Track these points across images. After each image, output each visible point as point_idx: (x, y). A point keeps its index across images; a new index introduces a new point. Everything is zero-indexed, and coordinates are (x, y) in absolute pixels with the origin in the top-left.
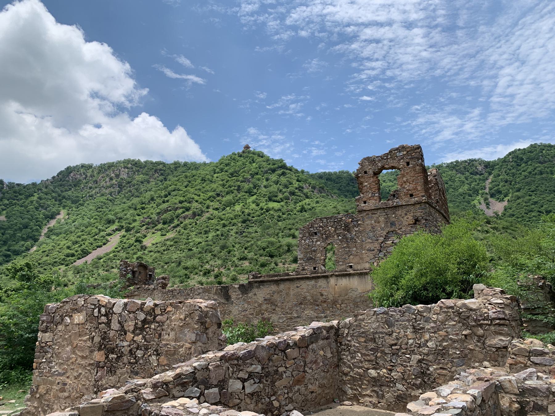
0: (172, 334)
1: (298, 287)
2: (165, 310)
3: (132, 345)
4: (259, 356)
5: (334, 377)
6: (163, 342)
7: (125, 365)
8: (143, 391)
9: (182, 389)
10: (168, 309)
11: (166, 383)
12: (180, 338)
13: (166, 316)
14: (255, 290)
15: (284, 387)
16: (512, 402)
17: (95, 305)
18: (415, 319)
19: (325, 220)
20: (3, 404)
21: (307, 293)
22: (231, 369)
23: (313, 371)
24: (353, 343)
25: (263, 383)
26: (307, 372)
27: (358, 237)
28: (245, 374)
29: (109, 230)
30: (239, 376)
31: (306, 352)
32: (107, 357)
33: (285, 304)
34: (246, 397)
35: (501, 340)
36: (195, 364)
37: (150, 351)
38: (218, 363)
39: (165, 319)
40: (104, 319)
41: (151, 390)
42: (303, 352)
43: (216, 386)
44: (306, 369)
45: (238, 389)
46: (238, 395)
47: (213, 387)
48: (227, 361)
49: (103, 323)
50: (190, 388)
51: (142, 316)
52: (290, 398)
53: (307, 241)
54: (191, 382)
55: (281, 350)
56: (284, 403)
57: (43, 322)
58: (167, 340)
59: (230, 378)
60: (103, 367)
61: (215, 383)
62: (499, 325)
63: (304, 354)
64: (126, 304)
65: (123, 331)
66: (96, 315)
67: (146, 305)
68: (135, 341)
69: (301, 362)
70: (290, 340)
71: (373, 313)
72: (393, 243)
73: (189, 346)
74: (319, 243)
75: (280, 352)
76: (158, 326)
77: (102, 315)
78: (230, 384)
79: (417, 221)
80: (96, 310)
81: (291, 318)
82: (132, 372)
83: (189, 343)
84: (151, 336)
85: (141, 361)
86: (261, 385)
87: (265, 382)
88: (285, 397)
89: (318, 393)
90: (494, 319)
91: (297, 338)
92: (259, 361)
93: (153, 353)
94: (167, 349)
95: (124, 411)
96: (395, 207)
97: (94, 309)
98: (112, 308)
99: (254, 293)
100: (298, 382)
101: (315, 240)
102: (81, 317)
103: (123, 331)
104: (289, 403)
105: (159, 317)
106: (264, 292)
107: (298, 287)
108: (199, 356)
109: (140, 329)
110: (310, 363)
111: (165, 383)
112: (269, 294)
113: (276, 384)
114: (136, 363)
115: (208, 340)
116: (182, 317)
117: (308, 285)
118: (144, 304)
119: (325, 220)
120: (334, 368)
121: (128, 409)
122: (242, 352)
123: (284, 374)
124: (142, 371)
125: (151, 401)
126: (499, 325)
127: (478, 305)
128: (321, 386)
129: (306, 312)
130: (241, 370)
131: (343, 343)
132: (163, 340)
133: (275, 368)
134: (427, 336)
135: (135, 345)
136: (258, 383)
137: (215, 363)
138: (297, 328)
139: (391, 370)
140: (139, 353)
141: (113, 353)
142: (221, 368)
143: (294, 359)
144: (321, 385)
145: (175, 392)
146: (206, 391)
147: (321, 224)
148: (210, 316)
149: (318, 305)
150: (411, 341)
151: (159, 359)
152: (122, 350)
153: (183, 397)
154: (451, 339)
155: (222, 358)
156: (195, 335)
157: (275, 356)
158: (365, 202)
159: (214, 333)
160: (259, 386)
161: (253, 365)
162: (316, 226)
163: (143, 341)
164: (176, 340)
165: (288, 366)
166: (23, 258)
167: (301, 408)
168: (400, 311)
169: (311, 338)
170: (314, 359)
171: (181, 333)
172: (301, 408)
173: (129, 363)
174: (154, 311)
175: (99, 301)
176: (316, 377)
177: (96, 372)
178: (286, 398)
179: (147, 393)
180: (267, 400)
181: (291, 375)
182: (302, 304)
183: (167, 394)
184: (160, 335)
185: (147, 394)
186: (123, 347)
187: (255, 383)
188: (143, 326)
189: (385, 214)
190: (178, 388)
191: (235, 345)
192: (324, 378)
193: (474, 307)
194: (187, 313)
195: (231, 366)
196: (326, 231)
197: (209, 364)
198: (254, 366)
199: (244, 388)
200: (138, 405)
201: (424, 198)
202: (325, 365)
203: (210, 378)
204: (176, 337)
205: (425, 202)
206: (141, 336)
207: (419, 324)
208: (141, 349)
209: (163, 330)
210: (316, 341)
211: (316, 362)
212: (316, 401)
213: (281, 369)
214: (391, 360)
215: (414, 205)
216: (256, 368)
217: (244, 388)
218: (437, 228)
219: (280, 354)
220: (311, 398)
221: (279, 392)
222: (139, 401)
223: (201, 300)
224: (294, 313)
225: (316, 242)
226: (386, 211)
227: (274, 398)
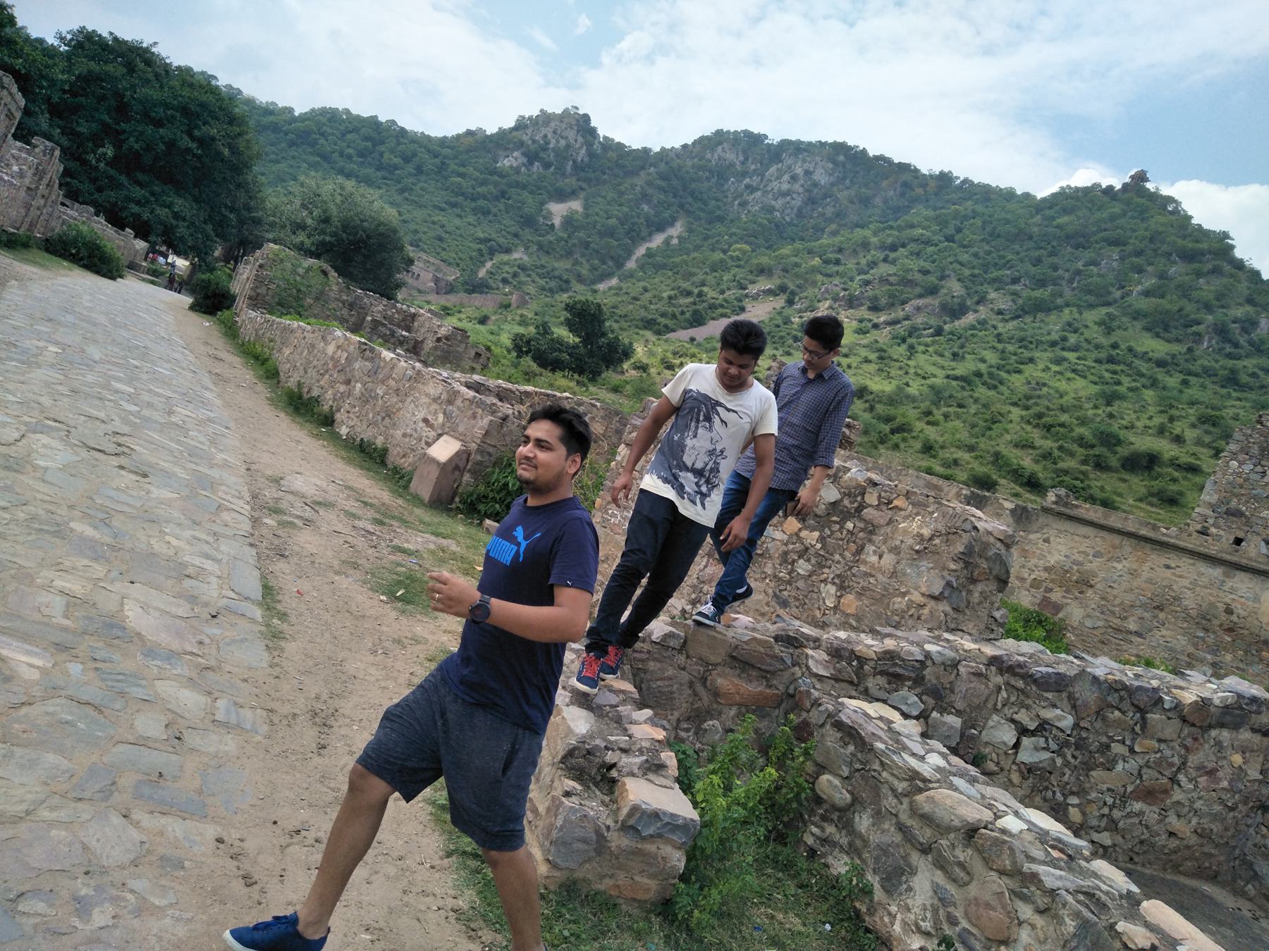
0: (888, 560)
1: (1168, 567)
2: (890, 502)
3: (793, 543)
4: (1077, 695)
5: (1243, 827)
6: (863, 568)
7: (765, 578)
8: (810, 652)
9: (887, 686)
10: (896, 503)
12: (905, 574)
15: (1109, 790)
20: (365, 503)
21: (1189, 592)
22: (1004, 694)
23: (1195, 790)
25: (1064, 756)
26: (1180, 786)
28: (1031, 719)
29: (753, 289)
30: (1016, 717)
31: (1195, 739)
33: (1115, 592)
34: (1014, 767)
37: (828, 573)
38: (983, 668)
39: (882, 522)
41: (826, 658)
42: (1189, 735)
43: (959, 713)
45: (1005, 744)
46: (998, 755)
47: (952, 713)
48: (1001, 671)
50: (904, 692)
52: (1113, 821)
54: (909, 679)
55: (1136, 707)
56: (1094, 822)
58: (873, 567)
59: (996, 710)
63: (1189, 742)
67: (849, 475)
69: (1173, 756)
70: (1167, 694)
73: (921, 600)
75: (1132, 708)
76: (862, 530)
78: (991, 723)
81: (1118, 630)
82: (775, 595)
83: (923, 595)
84: (841, 543)
85: (801, 584)
86: (1059, 761)
87: (1069, 758)
88: (1102, 812)
89: (1185, 842)
92: (1074, 707)
93: (833, 579)
94: (865, 584)
95: (764, 674)
99: (1045, 536)
100: (1149, 795)
104: (1106, 829)
106: (1072, 544)
107: (1168, 567)
108: (937, 633)
110: (1198, 769)
111: (858, 658)
112: (1082, 552)
113: (1093, 773)
114: (789, 583)
115: (967, 607)
116: (926, 532)
117: (1200, 574)
120: (1253, 807)
121: (773, 673)
122: (1044, 669)
123: (1121, 762)
124: (797, 604)
125: (820, 678)
128: (1200, 833)
129: (1164, 632)
130: (1028, 708)
132: (865, 563)
133: (1104, 740)
136: (1053, 752)
137: (974, 665)
138: (1188, 672)
140: (803, 567)
142: (984, 681)
143: (1160, 741)
144: (1204, 829)
145: (872, 683)
146: (935, 714)
148: (991, 557)
149: (1206, 630)
151: (840, 597)
152: (769, 545)
153: (884, 702)
155: (994, 661)
156: (943, 583)
157: (1117, 713)
159: (985, 598)
160: (1053, 760)
161: (1057, 708)
163: (819, 546)
164: (894, 574)
165: (1137, 749)
166: (1146, 353)
167: (1131, 854)
169: (1224, 714)
170: (1210, 766)
171: (911, 566)
172: (1131, 854)
173: (775, 576)
174: (863, 494)
176: (1198, 804)
177: (704, 563)
178: (1103, 815)
180: (1059, 797)
181: (1135, 773)
182: (1162, 610)
183: (856, 680)
184: (860, 550)
185: (817, 661)
186: (774, 539)
187: (1046, 749)
190: (881, 680)
191: (1023, 643)
192: (1215, 817)
194: (940, 528)
195: (1008, 688)
197: (959, 661)
198: (1058, 712)
199: (1017, 746)
200: (793, 674)
202: (1231, 790)
203: (952, 691)
204: (895, 568)
206: (816, 534)
208: (808, 560)
209: (870, 541)
210: (1236, 727)
211: (1211, 773)
212: (1173, 857)
213: (1117, 749)
216: (1059, 718)
217: (1017, 746)
219: (1131, 714)
220: (1164, 846)
221: (1093, 795)
222: (797, 668)
224: (1131, 619)
227: (1074, 800)
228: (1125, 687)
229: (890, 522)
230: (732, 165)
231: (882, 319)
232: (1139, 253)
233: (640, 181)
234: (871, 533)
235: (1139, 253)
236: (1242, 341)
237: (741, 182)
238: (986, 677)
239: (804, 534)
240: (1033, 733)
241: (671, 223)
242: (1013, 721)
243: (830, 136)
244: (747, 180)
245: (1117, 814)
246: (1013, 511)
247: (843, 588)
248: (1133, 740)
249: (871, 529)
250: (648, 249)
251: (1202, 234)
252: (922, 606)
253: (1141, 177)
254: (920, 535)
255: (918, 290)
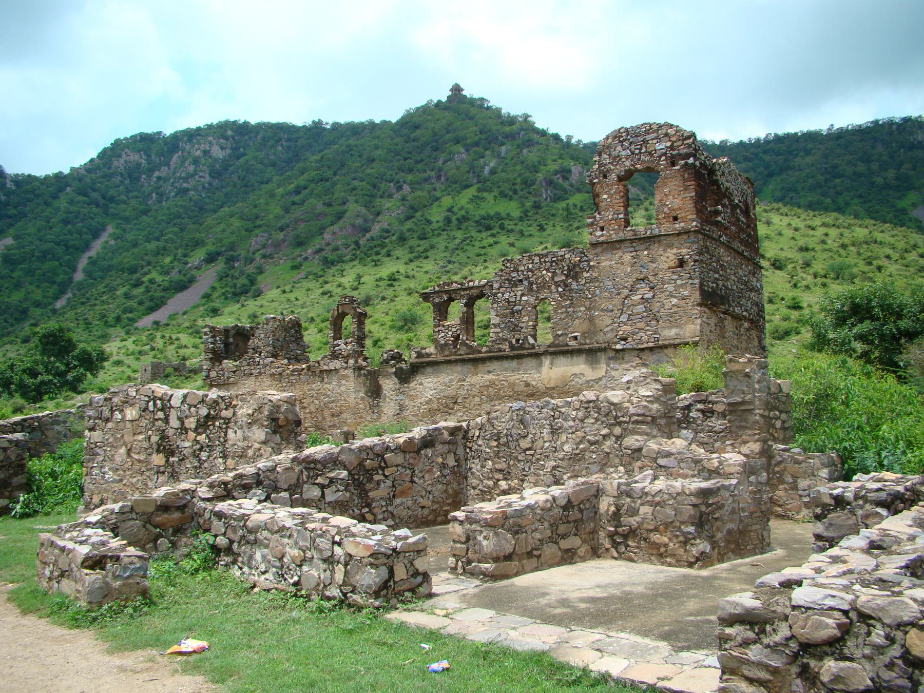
1: (489, 372)
11: (226, 484)
13: (231, 410)
14: (419, 378)
16: (609, 505)
17: (149, 397)
18: (553, 416)
19: (537, 259)
22: (305, 473)
24: (483, 448)
25: (350, 491)
27: (588, 290)
31: (415, 459)
32: (167, 461)
35: (637, 440)
36: (260, 465)
40: (160, 414)
43: (285, 490)
44: (415, 479)
49: (160, 419)
51: (204, 411)
53: (507, 295)
57: (90, 418)
59: (305, 483)
60: (163, 473)
61: (285, 487)
62: (637, 422)
64: (185, 396)
65: (183, 430)
66: (151, 409)
68: (198, 442)
71: (507, 409)
72: (642, 298)
74: (525, 298)
77: (159, 410)
78: (304, 489)
79: (681, 263)
80: (151, 403)
86: (348, 495)
90: (634, 415)
91: (401, 440)
96: (649, 238)
97: (148, 402)
98: (169, 400)
101: (519, 293)
102: (134, 412)
103: (183, 430)
105: (224, 411)
109: (203, 424)
118: (207, 396)
119: (537, 259)
126: (637, 422)
127: (620, 398)
131: (474, 448)
134: (564, 438)
135: (198, 446)
139: (523, 481)
140: (204, 456)
141: (173, 456)
147: (530, 266)
150: (547, 444)
154: (589, 441)
158: (602, 229)
162: (522, 268)
164: (245, 439)
168: (538, 407)
175: (153, 392)
179: (204, 492)
187: (338, 490)
188: (206, 423)
189: (632, 249)
193: (615, 400)
196: (537, 279)
199: (323, 493)
201: (694, 224)
205: (695, 231)
206: (204, 435)
207: (557, 423)
214: (524, 469)
215: (679, 234)
217: (323, 493)
218: (718, 273)
221: (374, 505)
223: (274, 392)
225: (523, 295)
226: (634, 244)
228: (367, 448)
229: (234, 414)
230: (139, 165)
231: (310, 251)
232: (477, 144)
233: (62, 203)
234: (229, 423)
235: (477, 144)
236: (566, 185)
237: (152, 176)
238: (292, 468)
239: (198, 438)
240: (329, 486)
241: (104, 229)
242: (317, 484)
243: (215, 117)
244: (157, 174)
245: (390, 508)
246: (395, 373)
247: (225, 457)
248: (383, 471)
249: (227, 421)
250: (90, 258)
251: (511, 120)
252: (260, 449)
253: (457, 89)
254: (248, 415)
255: (329, 219)
